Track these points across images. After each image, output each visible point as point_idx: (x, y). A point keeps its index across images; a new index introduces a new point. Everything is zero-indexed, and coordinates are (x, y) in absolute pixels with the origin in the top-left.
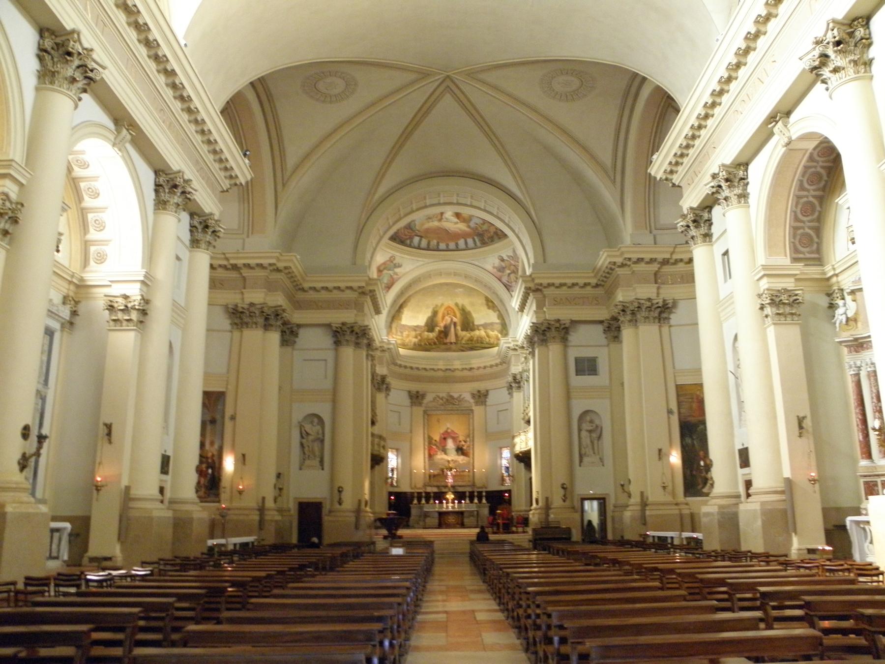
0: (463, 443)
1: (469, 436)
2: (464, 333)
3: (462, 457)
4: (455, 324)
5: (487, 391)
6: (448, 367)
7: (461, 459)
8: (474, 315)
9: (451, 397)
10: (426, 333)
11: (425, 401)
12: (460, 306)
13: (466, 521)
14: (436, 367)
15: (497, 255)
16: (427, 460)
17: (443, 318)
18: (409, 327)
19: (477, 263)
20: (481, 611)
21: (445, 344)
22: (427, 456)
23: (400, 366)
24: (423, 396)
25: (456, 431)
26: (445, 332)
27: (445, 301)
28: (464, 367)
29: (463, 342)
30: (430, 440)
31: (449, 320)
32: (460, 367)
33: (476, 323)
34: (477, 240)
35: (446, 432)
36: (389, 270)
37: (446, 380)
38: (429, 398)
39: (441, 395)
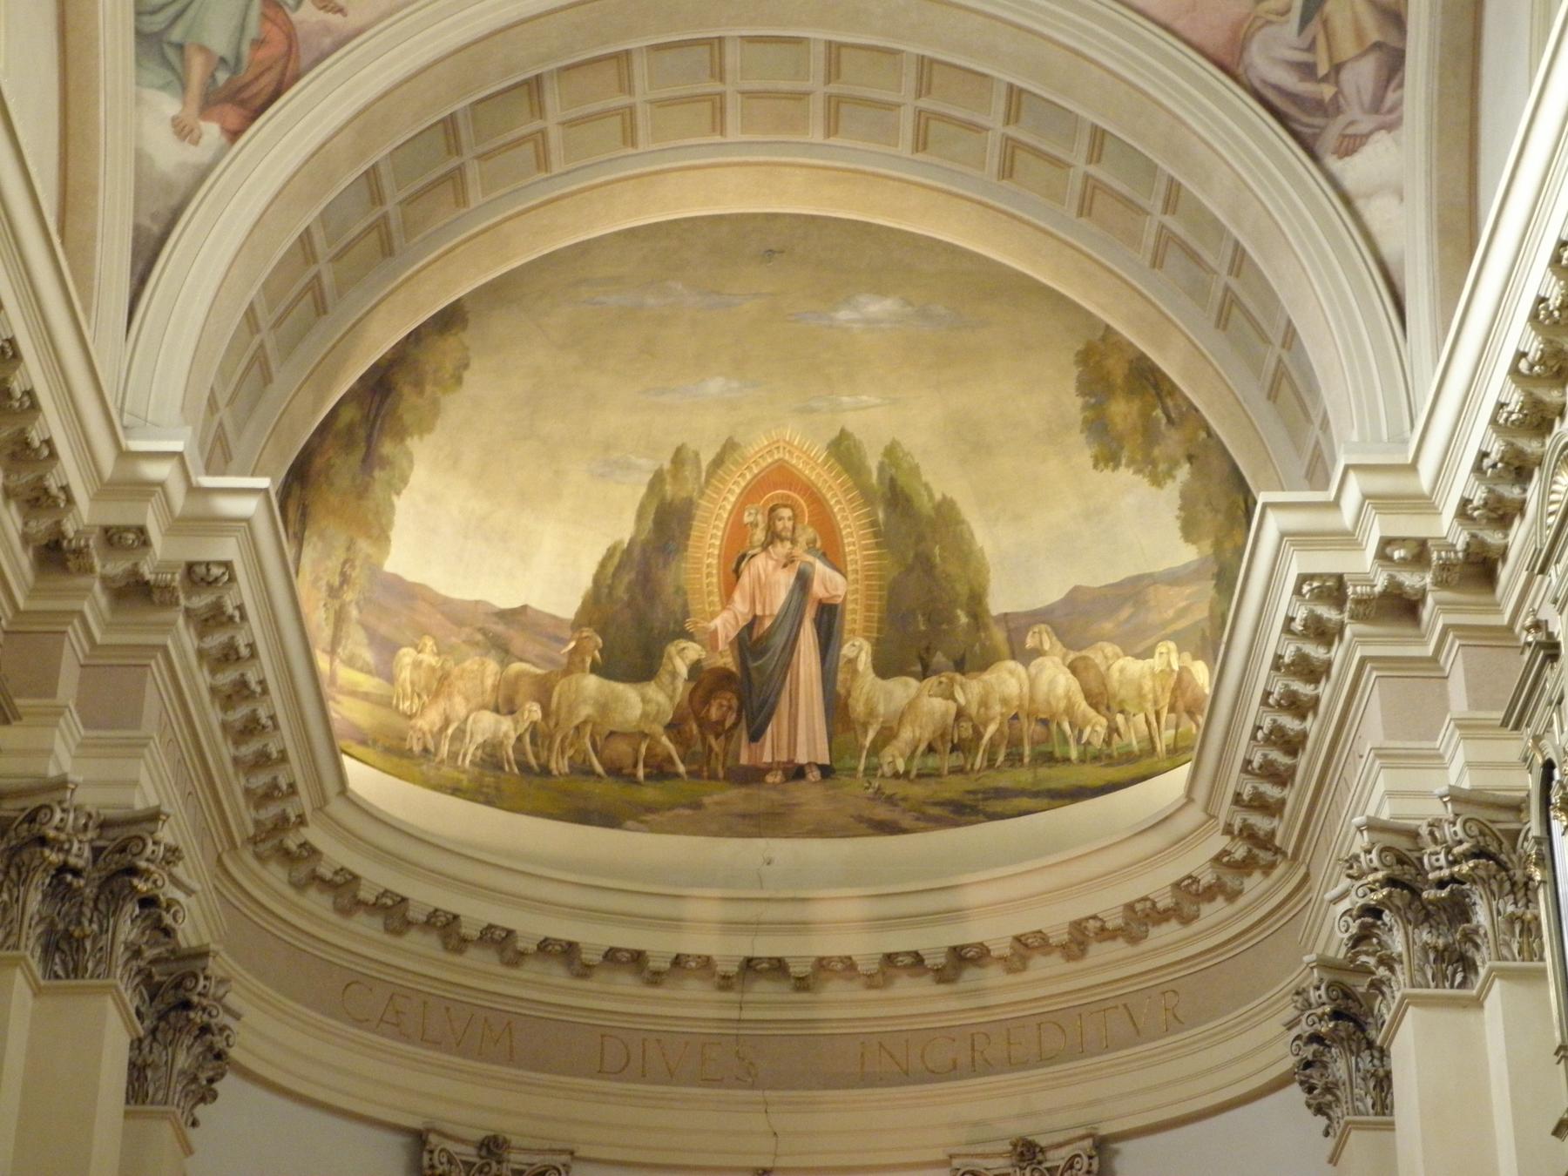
2: (902, 689)
4: (828, 619)
6: (765, 947)
8: (989, 537)
10: (592, 683)
14: (659, 946)
18: (455, 614)
21: (752, 776)
23: (343, 887)
27: (762, 418)
28: (899, 942)
29: (894, 758)
31: (784, 582)
32: (864, 947)
33: (999, 602)
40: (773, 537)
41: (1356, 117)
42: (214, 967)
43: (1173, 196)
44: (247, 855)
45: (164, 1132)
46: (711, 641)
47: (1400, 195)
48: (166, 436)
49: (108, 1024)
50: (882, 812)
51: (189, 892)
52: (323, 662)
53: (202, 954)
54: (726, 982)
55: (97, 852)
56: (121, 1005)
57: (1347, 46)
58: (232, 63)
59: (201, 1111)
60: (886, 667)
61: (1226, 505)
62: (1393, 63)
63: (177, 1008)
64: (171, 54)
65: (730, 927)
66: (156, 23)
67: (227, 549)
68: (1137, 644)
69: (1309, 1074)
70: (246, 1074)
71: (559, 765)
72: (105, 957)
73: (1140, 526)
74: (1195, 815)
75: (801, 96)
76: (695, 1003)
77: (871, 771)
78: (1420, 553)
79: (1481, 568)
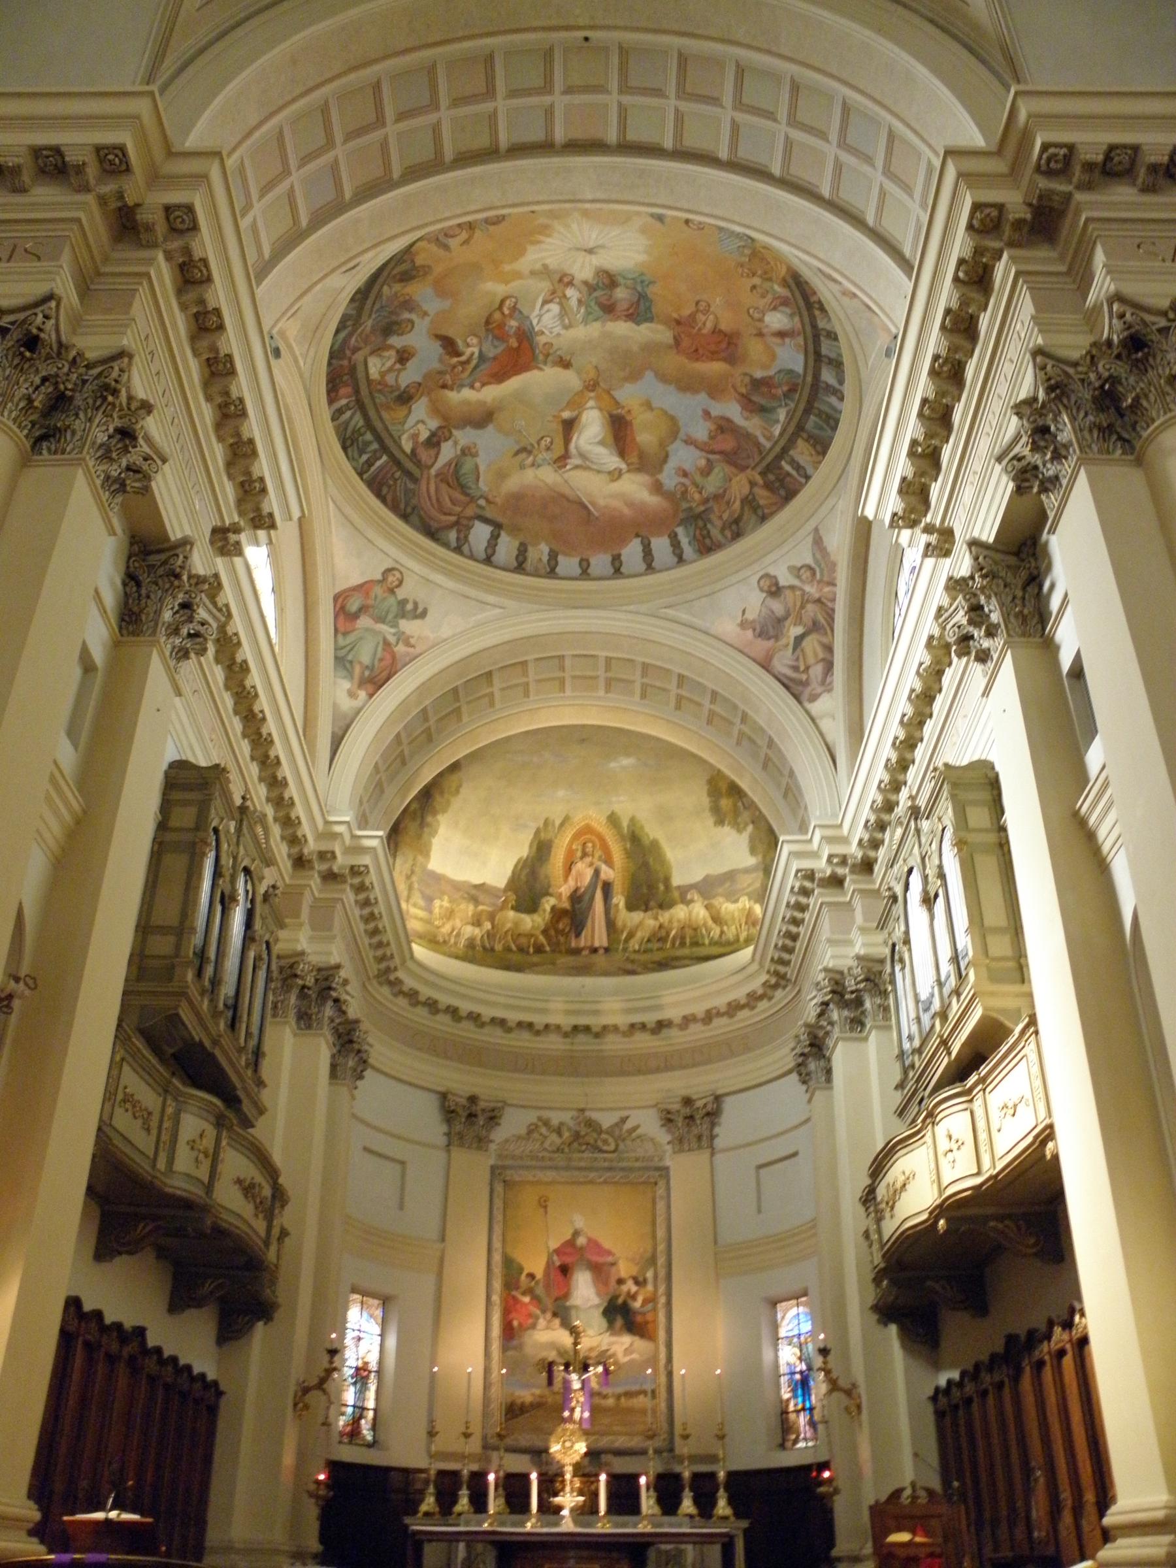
1: (652, 1261)
2: (637, 916)
3: (626, 1340)
4: (607, 888)
5: (718, 1099)
6: (583, 1021)
7: (623, 1346)
8: (672, 854)
9: (590, 1123)
10: (511, 914)
11: (499, 1135)
14: (539, 1020)
16: (496, 1346)
17: (568, 868)
18: (457, 886)
19: (684, 616)
20: (416, 918)
21: (577, 952)
22: (496, 1331)
23: (412, 996)
24: (493, 1118)
25: (607, 1244)
27: (578, 807)
28: (637, 1018)
29: (634, 944)
30: (512, 1274)
31: (589, 874)
32: (622, 1021)
33: (676, 881)
34: (684, 541)
35: (571, 1243)
36: (381, 619)
37: (571, 1067)
38: (512, 1124)
39: (556, 1118)
41: (815, 687)
43: (745, 718)
44: (375, 982)
45: (344, 1091)
48: (343, 816)
49: (322, 1049)
50: (629, 966)
52: (404, 905)
53: (357, 1021)
54: (566, 1035)
55: (317, 980)
56: (327, 1043)
57: (811, 660)
58: (371, 668)
59: (359, 1083)
60: (631, 907)
62: (829, 666)
63: (347, 1040)
64: (348, 665)
65: (568, 1012)
66: (342, 653)
67: (366, 860)
68: (732, 897)
70: (373, 1068)
71: (498, 947)
73: (733, 849)
74: (755, 966)
75: (596, 677)
77: (625, 950)
78: (844, 861)
79: (867, 866)
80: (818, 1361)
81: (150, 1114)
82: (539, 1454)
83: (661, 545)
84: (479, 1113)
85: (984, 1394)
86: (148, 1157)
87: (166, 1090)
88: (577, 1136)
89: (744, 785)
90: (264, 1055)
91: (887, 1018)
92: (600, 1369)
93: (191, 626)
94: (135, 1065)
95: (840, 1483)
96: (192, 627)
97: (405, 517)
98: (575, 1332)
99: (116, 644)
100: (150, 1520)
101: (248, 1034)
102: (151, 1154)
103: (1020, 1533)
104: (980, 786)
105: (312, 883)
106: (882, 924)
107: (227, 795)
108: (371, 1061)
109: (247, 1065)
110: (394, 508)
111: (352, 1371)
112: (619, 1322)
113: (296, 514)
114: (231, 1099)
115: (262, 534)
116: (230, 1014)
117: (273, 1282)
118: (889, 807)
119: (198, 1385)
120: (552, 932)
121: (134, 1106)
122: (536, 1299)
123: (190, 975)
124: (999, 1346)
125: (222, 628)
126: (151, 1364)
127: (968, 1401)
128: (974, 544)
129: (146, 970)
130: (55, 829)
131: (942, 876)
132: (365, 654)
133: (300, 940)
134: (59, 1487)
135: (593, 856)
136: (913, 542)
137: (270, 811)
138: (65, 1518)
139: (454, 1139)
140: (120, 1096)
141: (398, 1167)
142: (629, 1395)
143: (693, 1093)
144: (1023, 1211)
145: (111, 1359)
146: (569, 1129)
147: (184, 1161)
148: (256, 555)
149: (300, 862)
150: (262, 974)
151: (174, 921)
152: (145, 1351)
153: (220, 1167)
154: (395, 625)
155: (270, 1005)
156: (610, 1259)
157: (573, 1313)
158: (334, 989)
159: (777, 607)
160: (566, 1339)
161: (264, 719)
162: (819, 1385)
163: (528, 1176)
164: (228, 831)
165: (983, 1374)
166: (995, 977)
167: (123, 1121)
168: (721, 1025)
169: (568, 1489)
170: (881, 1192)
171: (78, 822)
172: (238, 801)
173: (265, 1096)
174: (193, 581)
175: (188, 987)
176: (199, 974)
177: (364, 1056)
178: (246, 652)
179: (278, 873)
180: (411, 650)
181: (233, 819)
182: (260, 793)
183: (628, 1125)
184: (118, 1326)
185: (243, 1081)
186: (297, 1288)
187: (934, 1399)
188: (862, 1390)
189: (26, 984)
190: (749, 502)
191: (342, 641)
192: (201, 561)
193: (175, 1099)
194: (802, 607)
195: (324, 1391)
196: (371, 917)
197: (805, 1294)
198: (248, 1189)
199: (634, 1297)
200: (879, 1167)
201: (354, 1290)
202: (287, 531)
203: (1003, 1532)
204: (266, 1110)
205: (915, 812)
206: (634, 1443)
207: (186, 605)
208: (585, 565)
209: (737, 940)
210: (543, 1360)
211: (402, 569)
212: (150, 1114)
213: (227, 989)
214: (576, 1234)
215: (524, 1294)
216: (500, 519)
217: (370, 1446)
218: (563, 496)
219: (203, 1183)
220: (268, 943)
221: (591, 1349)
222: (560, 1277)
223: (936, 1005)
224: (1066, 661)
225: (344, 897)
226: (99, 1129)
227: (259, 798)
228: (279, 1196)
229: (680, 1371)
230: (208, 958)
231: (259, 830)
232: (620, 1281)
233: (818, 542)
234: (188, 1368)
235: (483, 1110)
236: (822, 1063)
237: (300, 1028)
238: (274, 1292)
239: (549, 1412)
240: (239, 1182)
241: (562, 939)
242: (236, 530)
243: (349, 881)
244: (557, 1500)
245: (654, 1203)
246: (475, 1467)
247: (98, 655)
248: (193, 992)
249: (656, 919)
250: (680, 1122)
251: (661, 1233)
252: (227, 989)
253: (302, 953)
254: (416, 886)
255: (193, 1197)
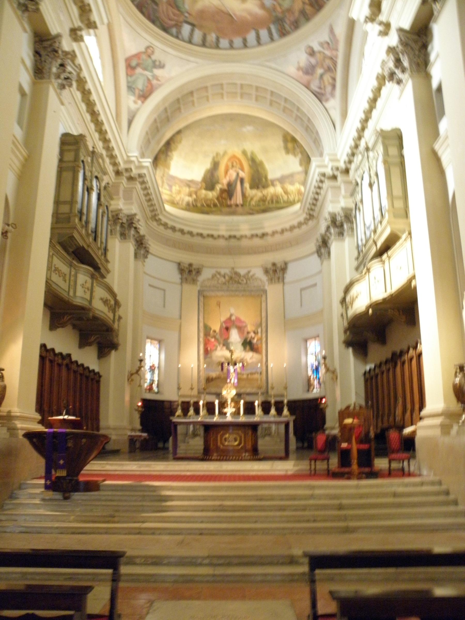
0: (252, 334)
2: (254, 192)
5: (286, 264)
6: (233, 233)
7: (249, 356)
8: (268, 166)
9: (237, 274)
10: (204, 192)
11: (201, 278)
12: (249, 154)
13: (262, 444)
14: (215, 233)
15: (303, 47)
17: (226, 172)
18: (181, 181)
19: (273, 65)
21: (230, 206)
23: (165, 225)
24: (198, 272)
25: (243, 318)
26: (229, 192)
27: (231, 147)
28: (254, 232)
29: (253, 203)
30: (207, 331)
32: (248, 233)
33: (271, 176)
35: (230, 319)
36: (145, 69)
37: (230, 252)
38: (206, 274)
39: (223, 271)
40: (233, 166)
41: (328, 96)
42: (146, 238)
43: (298, 109)
44: (150, 221)
45: (140, 263)
46: (223, 184)
47: (335, 109)
48: (134, 154)
49: (131, 247)
50: (251, 211)
51: (141, 226)
52: (160, 189)
53: (144, 236)
54: (226, 239)
55: (127, 220)
56: (132, 244)
57: (326, 83)
58: (142, 91)
59: (146, 260)
60: (251, 188)
61: (306, 160)
62: (334, 86)
63: (140, 243)
64: (133, 89)
65: (227, 230)
66: (130, 84)
67: (144, 171)
68: (292, 183)
69: (319, 253)
70: (152, 254)
71: (199, 205)
72: (129, 236)
73: (293, 164)
74: (301, 211)
75: (236, 93)
76: (222, 242)
77: (249, 205)
78: (337, 169)
79: (347, 171)
80: (322, 361)
81: (65, 275)
82: (219, 395)
83: (264, 33)
84: (193, 269)
85: (383, 373)
86: (66, 291)
87: (71, 265)
88: (231, 278)
89: (298, 137)
90: (108, 250)
91: (353, 235)
92: (241, 365)
93: (65, 74)
94: (58, 257)
95: (329, 403)
96: (66, 75)
97: (153, 22)
98: (231, 352)
99: (34, 84)
100: (79, 419)
101: (102, 242)
102: (67, 290)
103: (391, 419)
104: (394, 139)
105: (123, 182)
106: (352, 194)
107: (86, 147)
108: (150, 251)
109: (102, 254)
110: (149, 18)
111: (149, 367)
112: (248, 348)
113: (106, 21)
114: (96, 268)
115: (91, 31)
116: (94, 235)
117: (117, 336)
118: (357, 146)
119: (92, 374)
120: (220, 199)
121: (59, 272)
122: (216, 340)
123: (77, 220)
124: (390, 356)
125: (78, 75)
126: (74, 367)
127: (377, 376)
128: (401, 30)
129: (59, 219)
130: (17, 164)
131: (377, 175)
132: (140, 84)
133: (120, 205)
134: (46, 409)
135: (236, 167)
136: (373, 29)
137: (104, 153)
138: (49, 418)
139: (184, 280)
140: (53, 268)
141: (162, 292)
142: (252, 374)
143: (276, 261)
144: (401, 309)
145: (59, 365)
146: (228, 275)
147: (80, 292)
148: (90, 39)
149: (118, 173)
150: (105, 219)
151: (68, 198)
152: (72, 362)
153: (94, 294)
154: (151, 71)
155: (109, 231)
156: (244, 325)
157: (231, 345)
158: (134, 224)
159: (313, 61)
160: (228, 354)
161: (99, 114)
162: (322, 370)
163: (213, 294)
164: (88, 162)
165: (383, 365)
166: (396, 216)
167: (55, 278)
168: (287, 235)
169: (229, 406)
170: (348, 299)
171: (26, 160)
172: (91, 149)
173: (110, 266)
174: (64, 54)
175: (76, 225)
176: (80, 219)
177: (147, 249)
178: (89, 85)
179: (109, 178)
180: (159, 82)
181: (89, 156)
182: (100, 146)
183: (251, 274)
184: (61, 354)
185: (100, 260)
186: (126, 336)
187: (365, 374)
188: (338, 371)
189: (12, 227)
190: (303, 13)
191: (130, 79)
192: (66, 44)
193: (75, 269)
194: (324, 60)
195: (139, 375)
196: (148, 194)
197: (318, 336)
198: (105, 302)
199: (254, 338)
200: (347, 290)
201: (148, 338)
202: (102, 29)
203: (386, 418)
204: (110, 271)
205: (367, 149)
206: (254, 390)
207: (62, 65)
208: (231, 43)
209: (294, 200)
210: (219, 362)
211: (154, 47)
212: (65, 275)
213: (92, 225)
214: (231, 315)
215: (212, 338)
216: (195, 23)
217: (158, 393)
218: (222, 11)
219: (88, 300)
220: (107, 207)
221: (237, 358)
222: (225, 331)
223: (372, 227)
224: (435, 85)
225: (136, 187)
226: (47, 282)
227: (99, 147)
228: (117, 304)
229: (271, 365)
230: (84, 213)
231: (100, 161)
232: (248, 333)
233: (332, 31)
234: (88, 368)
235: (195, 269)
236: (327, 249)
237: (121, 239)
238: (117, 340)
239: (223, 380)
240: (102, 299)
241: (224, 201)
242: (80, 29)
243: (138, 180)
244: (225, 410)
245: (261, 303)
246: (195, 400)
247: (27, 88)
248: (79, 227)
249: (262, 192)
250: (271, 272)
251: (264, 314)
252: (92, 225)
253: (121, 210)
254: (165, 181)
255: (85, 306)
